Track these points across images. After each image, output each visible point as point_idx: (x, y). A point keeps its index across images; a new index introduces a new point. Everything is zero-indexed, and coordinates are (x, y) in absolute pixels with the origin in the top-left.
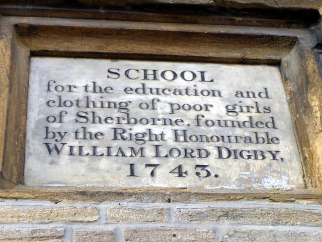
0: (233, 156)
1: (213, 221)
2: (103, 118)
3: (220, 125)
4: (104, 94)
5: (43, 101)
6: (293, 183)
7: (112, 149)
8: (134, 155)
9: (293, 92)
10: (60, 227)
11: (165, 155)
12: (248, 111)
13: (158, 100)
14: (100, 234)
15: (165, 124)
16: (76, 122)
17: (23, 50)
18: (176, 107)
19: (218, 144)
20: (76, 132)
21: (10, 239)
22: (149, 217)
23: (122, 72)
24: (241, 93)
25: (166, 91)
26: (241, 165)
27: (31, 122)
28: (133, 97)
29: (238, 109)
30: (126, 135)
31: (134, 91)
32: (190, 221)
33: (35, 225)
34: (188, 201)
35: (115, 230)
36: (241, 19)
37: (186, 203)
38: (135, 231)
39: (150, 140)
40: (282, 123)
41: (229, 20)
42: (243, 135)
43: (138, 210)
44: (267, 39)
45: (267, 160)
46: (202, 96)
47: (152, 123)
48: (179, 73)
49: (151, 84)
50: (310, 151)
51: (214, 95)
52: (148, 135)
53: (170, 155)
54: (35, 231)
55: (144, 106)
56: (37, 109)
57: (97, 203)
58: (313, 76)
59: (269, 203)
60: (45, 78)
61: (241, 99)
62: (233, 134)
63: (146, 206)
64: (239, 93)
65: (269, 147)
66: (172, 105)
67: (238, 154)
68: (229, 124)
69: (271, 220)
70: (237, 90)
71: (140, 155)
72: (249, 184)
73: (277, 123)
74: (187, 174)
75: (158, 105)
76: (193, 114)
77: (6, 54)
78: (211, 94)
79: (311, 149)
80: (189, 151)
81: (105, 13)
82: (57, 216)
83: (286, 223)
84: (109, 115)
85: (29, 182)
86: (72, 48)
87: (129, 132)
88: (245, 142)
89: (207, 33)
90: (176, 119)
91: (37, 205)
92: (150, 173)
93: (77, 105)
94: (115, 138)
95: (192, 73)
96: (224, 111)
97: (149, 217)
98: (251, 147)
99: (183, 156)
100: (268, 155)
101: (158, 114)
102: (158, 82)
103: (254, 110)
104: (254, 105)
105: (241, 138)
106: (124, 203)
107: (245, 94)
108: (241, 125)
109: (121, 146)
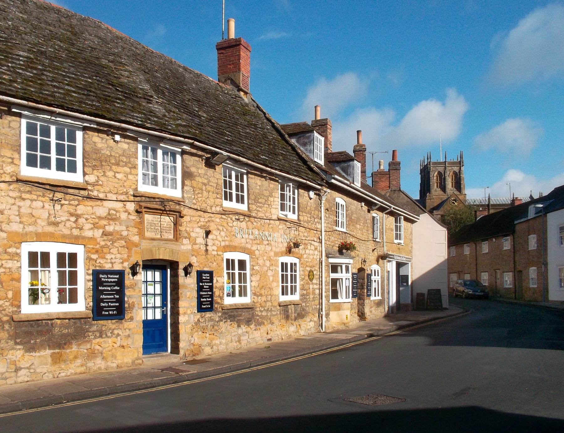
28: (156, 222)
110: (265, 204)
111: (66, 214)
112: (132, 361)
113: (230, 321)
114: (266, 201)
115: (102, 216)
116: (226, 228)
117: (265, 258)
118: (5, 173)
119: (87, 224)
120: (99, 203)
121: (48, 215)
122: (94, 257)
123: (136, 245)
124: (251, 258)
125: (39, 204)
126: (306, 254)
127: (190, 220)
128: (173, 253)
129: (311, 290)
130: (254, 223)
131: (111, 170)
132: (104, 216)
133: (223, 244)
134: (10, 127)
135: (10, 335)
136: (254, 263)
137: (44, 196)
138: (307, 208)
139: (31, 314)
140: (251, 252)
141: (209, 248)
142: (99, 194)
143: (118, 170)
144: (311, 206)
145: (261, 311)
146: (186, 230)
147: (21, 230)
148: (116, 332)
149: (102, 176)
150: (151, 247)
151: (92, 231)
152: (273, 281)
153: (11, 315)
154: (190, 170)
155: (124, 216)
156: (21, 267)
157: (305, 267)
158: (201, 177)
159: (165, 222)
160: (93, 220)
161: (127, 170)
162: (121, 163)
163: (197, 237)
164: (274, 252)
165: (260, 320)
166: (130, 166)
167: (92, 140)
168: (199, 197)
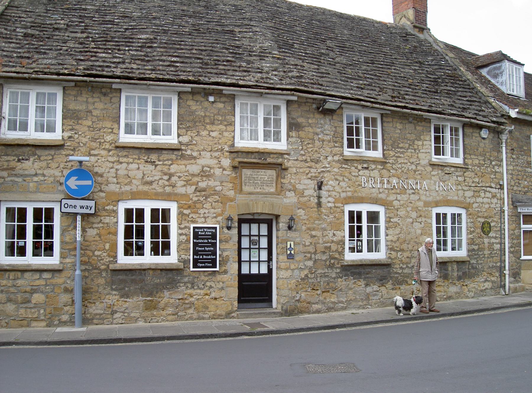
28: (255, 176)
49: (258, 174)
110: (409, 148)
111: (160, 173)
112: (226, 313)
113: (354, 279)
114: (410, 145)
115: (195, 173)
116: (348, 178)
117: (409, 209)
118: (105, 141)
119: (180, 182)
120: (193, 161)
121: (142, 175)
122: (186, 212)
123: (231, 200)
124: (386, 209)
125: (134, 166)
126: (477, 203)
127: (295, 172)
128: (273, 207)
129: (486, 245)
130: (391, 171)
131: (205, 129)
132: (197, 174)
133: (343, 195)
134: (111, 102)
135: (106, 282)
136: (392, 215)
137: (139, 159)
138: (477, 150)
139: (126, 264)
140: (386, 203)
141: (323, 200)
142: (193, 153)
143: (214, 129)
144: (485, 147)
145: (401, 268)
146: (290, 182)
147: (118, 190)
148: (208, 284)
149: (196, 135)
150: (248, 201)
151: (184, 188)
152: (422, 234)
153: (108, 264)
154: (297, 121)
155: (218, 172)
156: (117, 222)
157: (476, 218)
158: (312, 127)
159: (266, 175)
160: (186, 177)
161: (222, 127)
162: (216, 122)
163: (306, 189)
164: (424, 202)
165: (399, 278)
166: (226, 123)
167: (186, 104)
168: (309, 148)
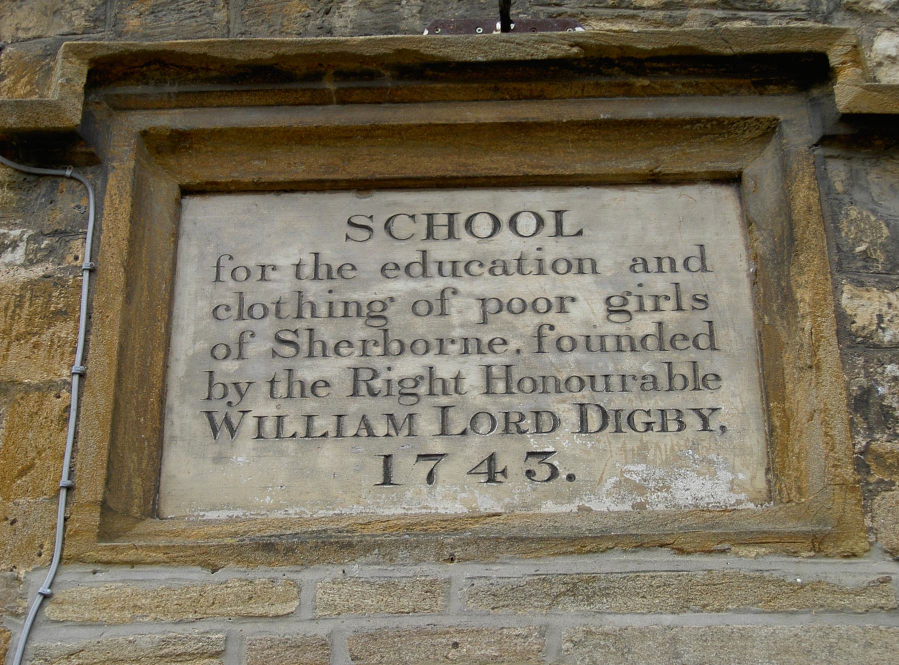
0: (611, 428)
1: (542, 607)
2: (331, 344)
3: (588, 348)
4: (337, 283)
5: (205, 307)
6: (742, 487)
7: (346, 421)
8: (393, 432)
9: (761, 257)
10: (218, 632)
11: (460, 430)
12: (657, 309)
13: (455, 292)
14: (300, 646)
15: (466, 352)
16: (273, 357)
17: (163, 184)
18: (492, 306)
19: (580, 397)
20: (272, 382)
21: (115, 661)
22: (404, 601)
23: (378, 225)
24: (645, 262)
25: (474, 268)
26: (629, 446)
27: (177, 360)
28: (400, 287)
29: (632, 306)
30: (378, 384)
31: (402, 272)
32: (493, 609)
33: (169, 628)
34: (493, 560)
35: (329, 636)
36: (646, 82)
37: (488, 563)
38: (371, 637)
39: (431, 393)
40: (732, 333)
41: (619, 85)
42: (640, 371)
43: (382, 586)
44: (709, 126)
45: (688, 433)
46: (553, 274)
47: (436, 351)
48: (504, 218)
49: (441, 251)
50: (784, 410)
51: (581, 271)
52: (427, 381)
53: (472, 428)
54: (166, 642)
55: (422, 308)
56: (192, 329)
57: (298, 568)
58: (803, 223)
59: (671, 558)
60: (210, 249)
61: (643, 277)
62: (617, 370)
63: (398, 575)
64: (640, 261)
65: (695, 399)
66: (484, 301)
67: (624, 420)
68: (610, 343)
69: (671, 601)
70: (634, 255)
71: (406, 432)
72: (642, 495)
73: (720, 333)
74: (506, 477)
75: (454, 303)
76: (530, 321)
77: (121, 210)
78: (575, 269)
79: (787, 405)
80: (515, 418)
81: (337, 91)
82: (213, 603)
83: (704, 606)
84: (344, 335)
85: (168, 509)
86: (271, 173)
87: (385, 375)
88: (643, 390)
89: (568, 122)
90: (490, 338)
91: (173, 579)
92: (425, 475)
93: (278, 311)
94: (355, 393)
95: (536, 214)
96: (600, 309)
97: (404, 601)
98: (656, 402)
99: (500, 431)
100: (694, 422)
101: (452, 327)
102: (457, 243)
103: (668, 305)
104: (671, 293)
105: (634, 378)
106: (355, 569)
107: (653, 265)
108: (637, 345)
109: (366, 413)
159: (577, 266)
